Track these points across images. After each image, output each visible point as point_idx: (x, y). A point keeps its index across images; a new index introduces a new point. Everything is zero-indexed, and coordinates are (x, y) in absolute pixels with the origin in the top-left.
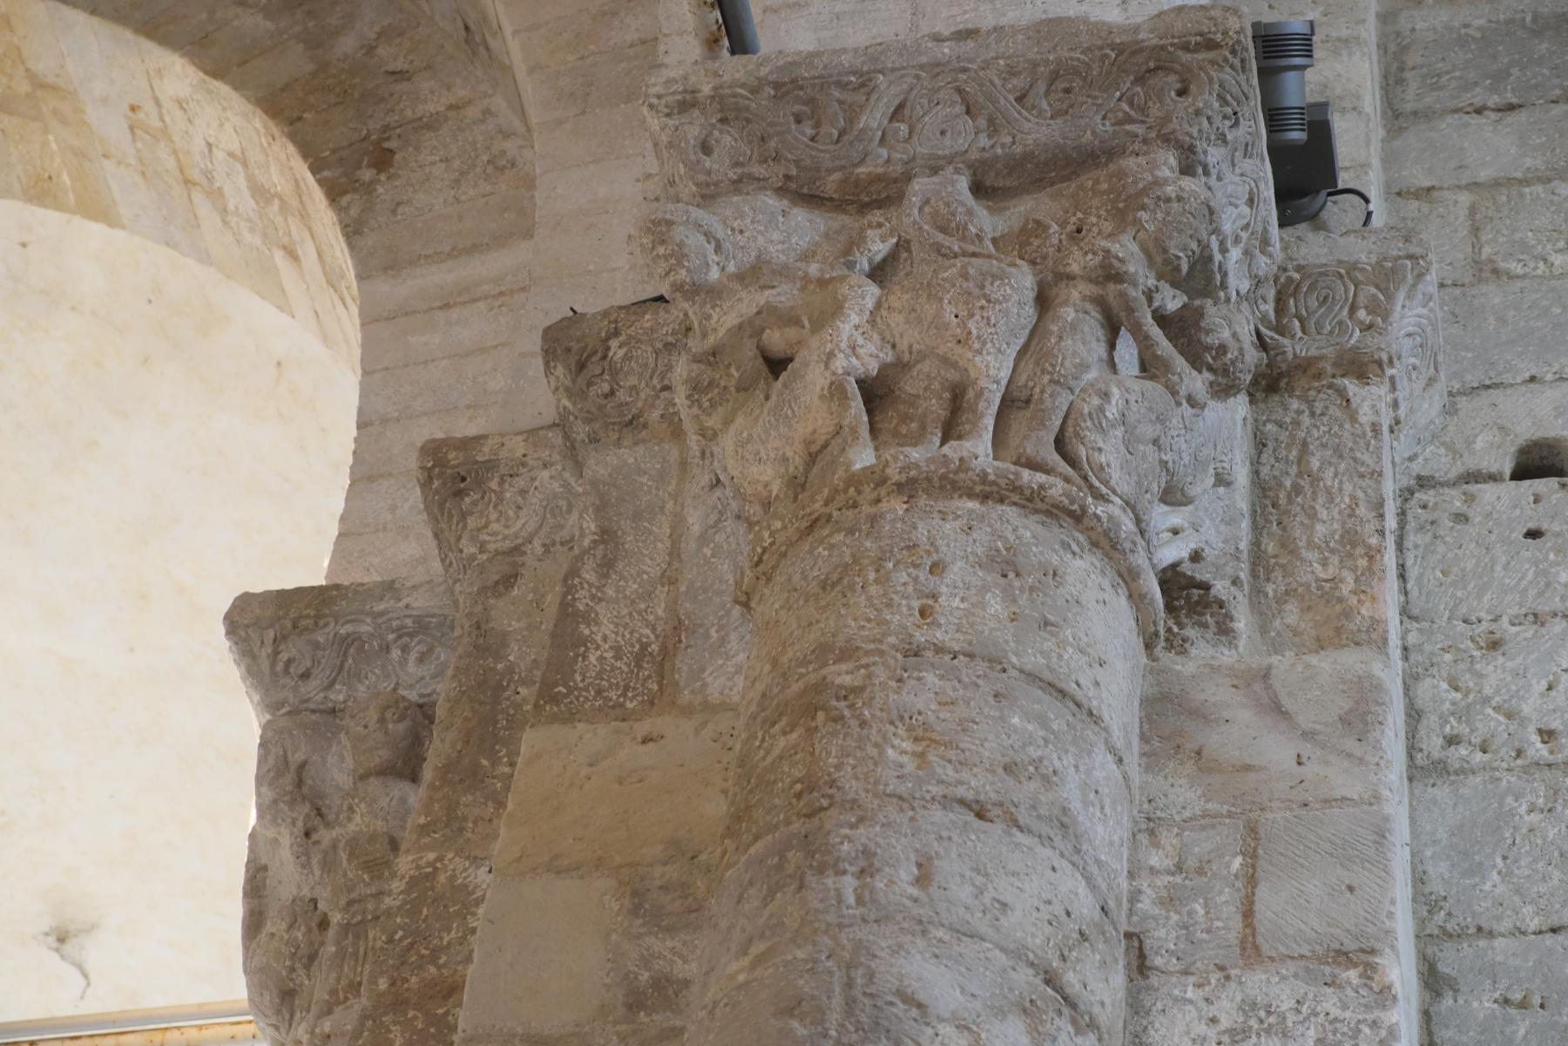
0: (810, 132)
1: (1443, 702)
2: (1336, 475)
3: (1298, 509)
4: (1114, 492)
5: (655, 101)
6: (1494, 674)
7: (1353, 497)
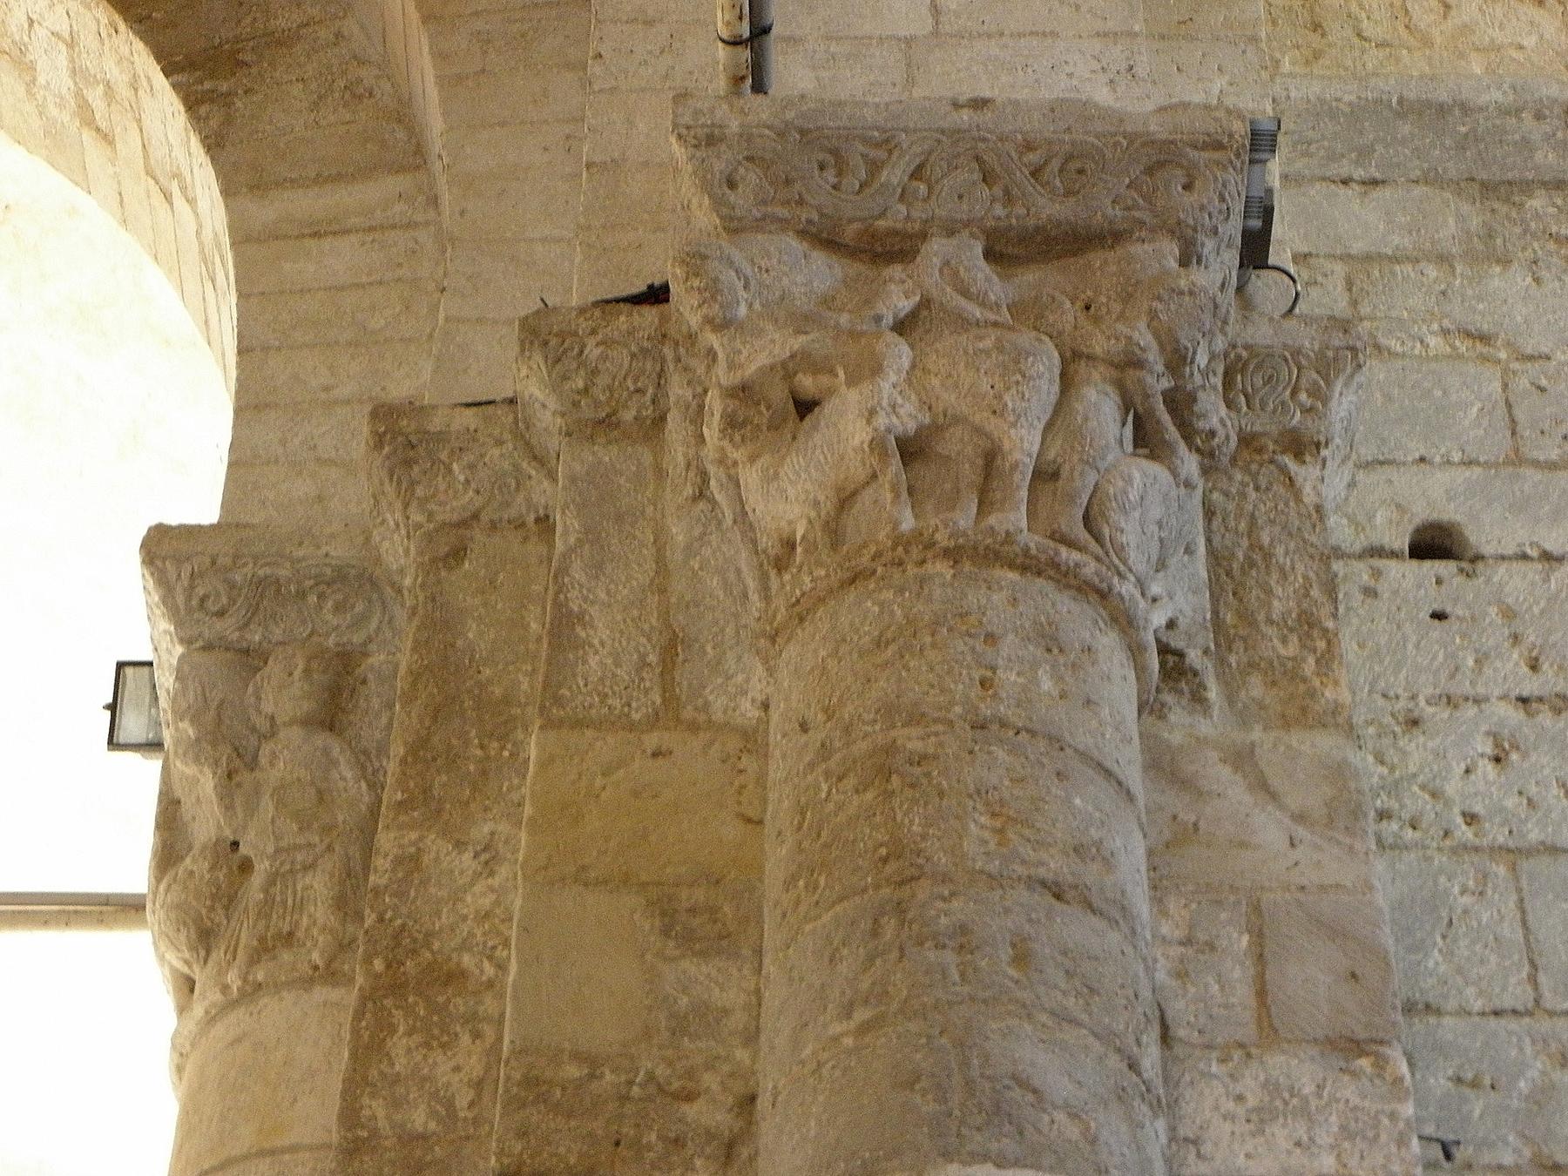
0: (833, 180)
1: (1371, 775)
2: (1287, 553)
3: (1253, 582)
4: (1130, 570)
5: (684, 132)
6: (1416, 751)
7: (1306, 577)
